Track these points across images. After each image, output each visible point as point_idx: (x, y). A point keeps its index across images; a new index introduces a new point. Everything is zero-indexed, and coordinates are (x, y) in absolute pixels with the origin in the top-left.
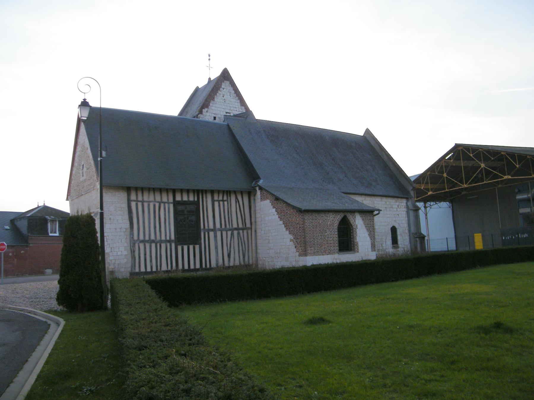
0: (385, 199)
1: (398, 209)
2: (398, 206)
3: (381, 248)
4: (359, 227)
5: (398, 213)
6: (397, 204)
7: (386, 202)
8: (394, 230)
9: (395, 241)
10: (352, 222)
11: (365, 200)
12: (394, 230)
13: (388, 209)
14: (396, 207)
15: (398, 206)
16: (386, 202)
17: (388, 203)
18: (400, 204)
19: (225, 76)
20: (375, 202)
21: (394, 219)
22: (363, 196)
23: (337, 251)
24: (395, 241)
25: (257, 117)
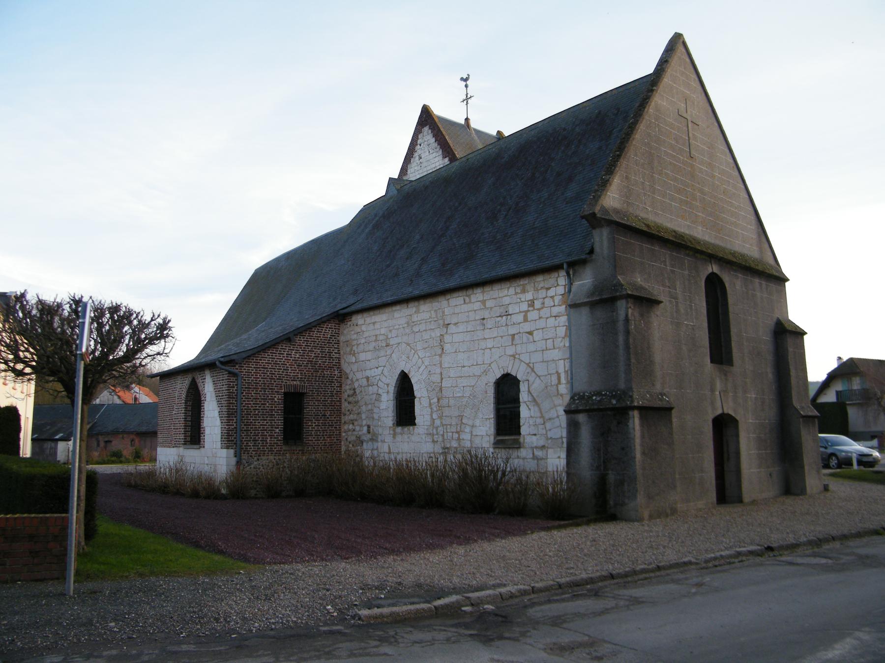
0: (478, 295)
1: (533, 315)
2: (531, 304)
3: (454, 444)
4: (208, 398)
5: (527, 327)
6: (529, 296)
7: (484, 302)
8: (507, 390)
9: (507, 421)
10: (200, 389)
11: (417, 312)
12: (507, 390)
13: (489, 324)
14: (524, 307)
15: (531, 304)
16: (484, 302)
17: (489, 304)
18: (542, 293)
19: (676, 43)
20: (447, 311)
21: (510, 351)
22: (411, 305)
23: (182, 441)
24: (507, 421)
25: (383, 192)
